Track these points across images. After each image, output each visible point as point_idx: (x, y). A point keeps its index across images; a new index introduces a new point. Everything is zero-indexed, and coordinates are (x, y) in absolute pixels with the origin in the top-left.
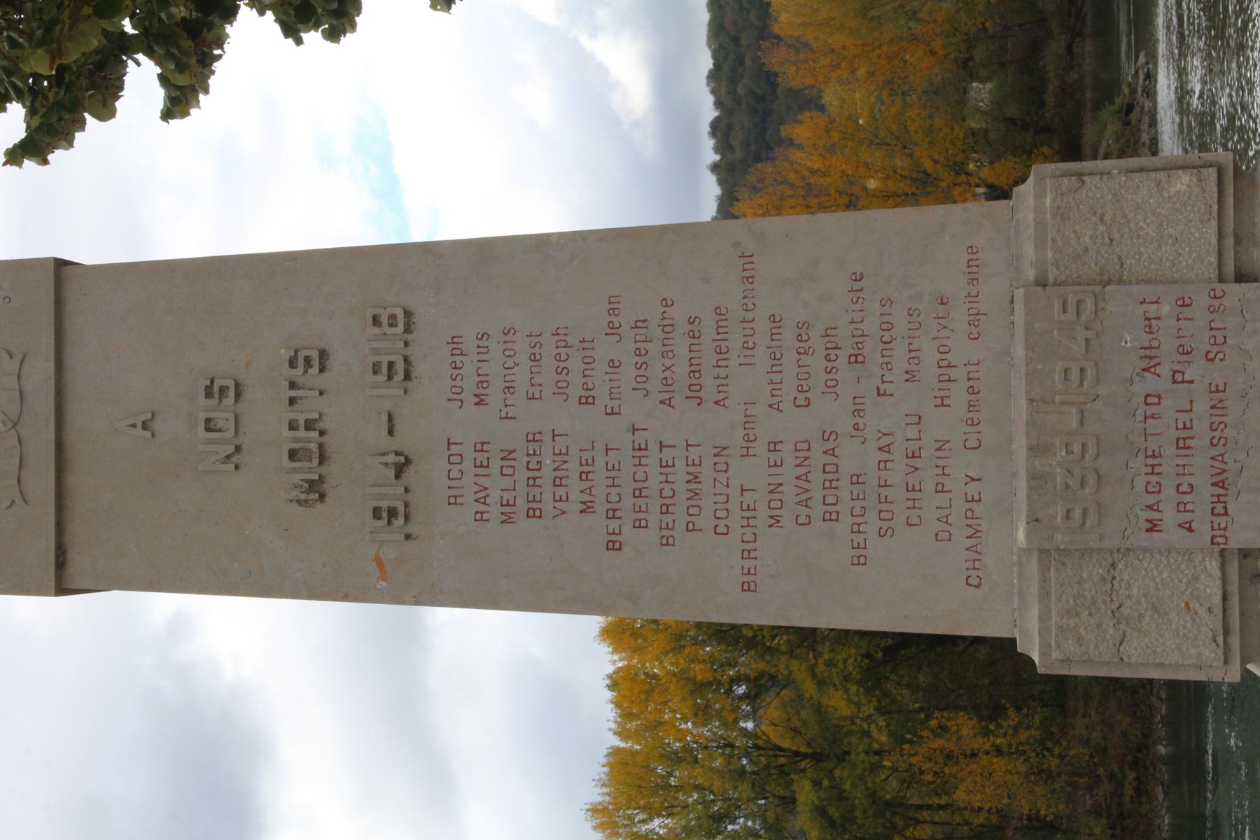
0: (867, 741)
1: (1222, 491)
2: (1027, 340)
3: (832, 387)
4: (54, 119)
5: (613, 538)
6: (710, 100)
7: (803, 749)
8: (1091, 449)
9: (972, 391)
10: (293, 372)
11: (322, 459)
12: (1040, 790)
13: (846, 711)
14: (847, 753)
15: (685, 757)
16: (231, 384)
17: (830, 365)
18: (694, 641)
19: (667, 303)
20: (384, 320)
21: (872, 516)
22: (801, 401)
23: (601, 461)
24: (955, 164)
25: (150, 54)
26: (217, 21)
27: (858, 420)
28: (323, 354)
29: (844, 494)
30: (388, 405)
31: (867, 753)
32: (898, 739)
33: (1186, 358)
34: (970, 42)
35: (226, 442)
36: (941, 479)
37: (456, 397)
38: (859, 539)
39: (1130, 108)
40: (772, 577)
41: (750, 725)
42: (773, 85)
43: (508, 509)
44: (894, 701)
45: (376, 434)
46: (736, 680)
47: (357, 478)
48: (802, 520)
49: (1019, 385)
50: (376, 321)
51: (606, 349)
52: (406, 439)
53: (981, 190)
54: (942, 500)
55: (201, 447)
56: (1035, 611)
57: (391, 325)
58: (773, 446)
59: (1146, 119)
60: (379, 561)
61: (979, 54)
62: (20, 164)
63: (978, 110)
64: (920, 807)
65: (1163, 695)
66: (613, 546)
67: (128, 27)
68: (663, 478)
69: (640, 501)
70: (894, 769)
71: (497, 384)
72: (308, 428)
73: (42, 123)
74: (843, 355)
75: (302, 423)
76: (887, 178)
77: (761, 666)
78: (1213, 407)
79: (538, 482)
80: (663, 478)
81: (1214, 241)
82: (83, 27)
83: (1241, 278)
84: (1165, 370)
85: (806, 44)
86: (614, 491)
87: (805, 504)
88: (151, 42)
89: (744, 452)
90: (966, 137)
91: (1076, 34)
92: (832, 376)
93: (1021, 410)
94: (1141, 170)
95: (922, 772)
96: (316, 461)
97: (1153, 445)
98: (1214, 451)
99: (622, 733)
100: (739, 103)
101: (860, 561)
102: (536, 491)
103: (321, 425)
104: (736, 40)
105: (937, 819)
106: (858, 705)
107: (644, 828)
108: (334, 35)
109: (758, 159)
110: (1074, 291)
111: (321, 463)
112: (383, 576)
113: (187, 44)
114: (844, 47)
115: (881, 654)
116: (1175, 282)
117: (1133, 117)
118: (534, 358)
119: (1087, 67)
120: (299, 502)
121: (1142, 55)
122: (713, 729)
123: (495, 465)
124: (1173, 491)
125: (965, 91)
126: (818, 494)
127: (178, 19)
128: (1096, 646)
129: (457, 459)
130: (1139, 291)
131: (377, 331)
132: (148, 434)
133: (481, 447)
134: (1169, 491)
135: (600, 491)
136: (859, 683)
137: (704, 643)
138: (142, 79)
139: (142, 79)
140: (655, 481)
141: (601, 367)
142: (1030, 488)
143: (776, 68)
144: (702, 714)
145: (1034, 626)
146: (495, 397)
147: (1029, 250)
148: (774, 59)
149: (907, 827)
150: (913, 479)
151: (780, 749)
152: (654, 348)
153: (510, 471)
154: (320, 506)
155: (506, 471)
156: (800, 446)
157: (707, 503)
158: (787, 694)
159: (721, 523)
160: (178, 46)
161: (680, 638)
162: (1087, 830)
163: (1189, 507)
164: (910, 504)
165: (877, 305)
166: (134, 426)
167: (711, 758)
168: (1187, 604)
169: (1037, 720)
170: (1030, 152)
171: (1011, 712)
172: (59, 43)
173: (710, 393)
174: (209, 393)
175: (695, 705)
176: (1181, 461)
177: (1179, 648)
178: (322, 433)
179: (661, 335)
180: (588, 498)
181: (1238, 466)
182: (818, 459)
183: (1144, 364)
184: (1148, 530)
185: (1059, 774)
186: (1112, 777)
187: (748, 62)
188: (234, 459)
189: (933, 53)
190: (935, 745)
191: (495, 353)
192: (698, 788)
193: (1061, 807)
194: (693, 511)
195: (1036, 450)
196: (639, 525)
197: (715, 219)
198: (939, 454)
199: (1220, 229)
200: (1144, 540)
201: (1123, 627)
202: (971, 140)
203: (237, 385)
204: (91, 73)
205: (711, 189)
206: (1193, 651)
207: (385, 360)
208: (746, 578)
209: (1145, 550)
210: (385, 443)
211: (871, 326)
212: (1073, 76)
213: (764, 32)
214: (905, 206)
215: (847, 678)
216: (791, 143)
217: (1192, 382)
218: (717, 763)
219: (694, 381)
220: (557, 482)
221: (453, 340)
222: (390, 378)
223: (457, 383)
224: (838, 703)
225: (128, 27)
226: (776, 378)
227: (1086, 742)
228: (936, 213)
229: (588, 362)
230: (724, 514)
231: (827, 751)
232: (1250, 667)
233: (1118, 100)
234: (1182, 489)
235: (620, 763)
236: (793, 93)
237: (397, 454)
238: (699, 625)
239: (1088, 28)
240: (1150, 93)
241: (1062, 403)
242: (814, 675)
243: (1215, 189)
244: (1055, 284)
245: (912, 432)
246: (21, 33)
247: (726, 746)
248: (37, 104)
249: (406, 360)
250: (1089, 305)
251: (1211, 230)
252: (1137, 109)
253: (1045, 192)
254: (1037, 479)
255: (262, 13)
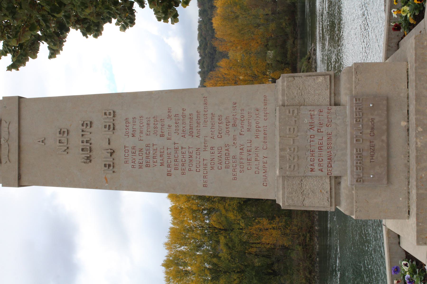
0: (238, 226)
1: (330, 161)
2: (279, 120)
3: (228, 133)
4: (20, 58)
5: (169, 172)
6: (198, 54)
7: (222, 228)
8: (296, 149)
9: (265, 134)
10: (83, 127)
11: (91, 151)
12: (285, 239)
13: (233, 218)
14: (233, 229)
15: (191, 230)
16: (66, 130)
17: (227, 127)
18: (193, 199)
19: (184, 110)
20: (108, 114)
21: (238, 167)
22: (219, 136)
23: (166, 152)
24: (263, 72)
25: (46, 41)
26: (65, 32)
27: (235, 141)
28: (91, 123)
29: (231, 161)
30: (108, 137)
31: (239, 229)
32: (247, 225)
33: (321, 125)
34: (268, 40)
35: (64, 146)
36: (256, 157)
37: (127, 134)
38: (235, 173)
39: (309, 58)
40: (211, 183)
41: (208, 222)
42: (215, 51)
43: (141, 165)
44: (246, 215)
45: (105, 144)
46: (203, 210)
47: (100, 156)
48: (219, 168)
49: (277, 133)
50: (105, 114)
51: (167, 122)
52: (113, 146)
53: (270, 79)
54: (257, 163)
55: (58, 148)
56: (281, 192)
57: (109, 115)
58: (212, 148)
59: (314, 61)
60: (106, 179)
61: (270, 43)
62: (11, 70)
63: (270, 58)
64: (253, 243)
65: (317, 213)
66: (169, 175)
67: (39, 33)
68: (182, 157)
69: (176, 163)
70: (246, 233)
71: (138, 131)
72: (87, 143)
73: (17, 60)
74: (231, 124)
75: (85, 141)
76: (245, 76)
77: (211, 206)
78: (328, 139)
79: (149, 157)
80: (182, 157)
81: (329, 95)
82: (26, 33)
83: (336, 105)
84: (315, 129)
85: (224, 40)
86: (169, 160)
87: (220, 164)
88: (46, 38)
89: (204, 150)
90: (266, 65)
91: (296, 38)
92: (228, 130)
93: (278, 139)
94: (310, 76)
95: (253, 234)
96: (89, 151)
97: (312, 148)
98: (328, 150)
99: (173, 223)
100: (206, 55)
101: (235, 179)
102: (148, 160)
103: (90, 142)
104: (205, 39)
105: (257, 246)
106: (236, 216)
107: (179, 249)
108: (96, 36)
109: (211, 71)
110: (291, 108)
111: (90, 152)
112: (107, 182)
113: (56, 38)
114: (234, 41)
115: (242, 202)
116: (318, 105)
117: (310, 61)
118: (148, 124)
119: (298, 47)
120: (84, 162)
121: (313, 44)
122: (196, 223)
123: (137, 153)
124: (318, 161)
125: (266, 53)
126: (224, 161)
127: (52, 32)
128: (297, 202)
129: (127, 151)
130: (309, 108)
131: (106, 116)
132: (43, 144)
133: (133, 148)
134: (316, 161)
135: (166, 160)
136: (237, 211)
137: (195, 200)
138: (44, 48)
139: (44, 48)
140: (180, 157)
141: (166, 127)
142: (280, 160)
143: (216, 46)
144: (195, 218)
145: (281, 196)
146: (137, 134)
147: (280, 97)
148: (215, 44)
149: (249, 248)
150: (249, 157)
151: (216, 228)
152: (180, 122)
153: (141, 154)
154: (90, 163)
155: (140, 154)
156: (219, 148)
157: (194, 163)
158: (218, 213)
159: (198, 169)
160: (54, 39)
161: (189, 198)
162: (297, 249)
163: (322, 165)
164: (248, 164)
165: (240, 111)
166: (39, 142)
167: (197, 230)
168: (321, 191)
169: (284, 220)
170: (283, 70)
171: (277, 218)
172: (19, 38)
173: (195, 134)
174: (60, 133)
175: (193, 216)
176: (319, 153)
177: (319, 202)
178: (90, 144)
179: (182, 118)
180: (162, 162)
181: (335, 154)
182: (224, 152)
183: (310, 127)
184: (311, 171)
185: (289, 235)
186: (303, 235)
187: (209, 45)
188: (67, 151)
189: (258, 43)
190: (257, 227)
191: (138, 123)
192: (193, 238)
193: (290, 243)
194: (190, 165)
195: (281, 150)
196: (176, 169)
197: (199, 87)
198: (256, 150)
199: (330, 92)
200: (310, 174)
201: (304, 196)
202: (268, 66)
203: (68, 131)
204: (30, 46)
205: (198, 78)
206: (322, 203)
207: (108, 124)
208: (205, 183)
209: (310, 176)
210: (107, 146)
211: (238, 117)
212: (295, 50)
213: (213, 37)
214: (250, 84)
215: (234, 209)
216: (220, 67)
217: (322, 132)
218: (199, 232)
219: (191, 131)
220: (154, 157)
221: (126, 119)
222: (109, 129)
223: (127, 131)
224: (231, 216)
225: (39, 33)
226: (213, 130)
227: (297, 226)
228: (256, 86)
229: (163, 125)
230: (199, 166)
231: (228, 229)
232: (337, 207)
233: (306, 56)
234: (320, 160)
235: (173, 231)
236: (221, 53)
237: (111, 149)
238: (194, 196)
239: (299, 37)
240: (315, 54)
241: (289, 137)
242: (225, 208)
243: (329, 81)
244: (287, 106)
245: (249, 145)
246: (11, 35)
247: (201, 227)
248: (15, 54)
249: (114, 124)
250: (296, 111)
251: (328, 92)
252: (311, 59)
253: (284, 81)
254: (282, 157)
255: (77, 30)
